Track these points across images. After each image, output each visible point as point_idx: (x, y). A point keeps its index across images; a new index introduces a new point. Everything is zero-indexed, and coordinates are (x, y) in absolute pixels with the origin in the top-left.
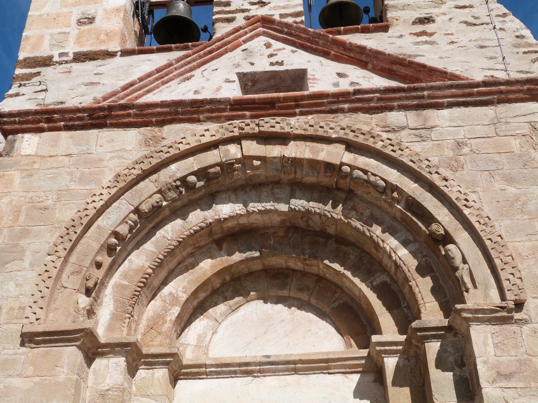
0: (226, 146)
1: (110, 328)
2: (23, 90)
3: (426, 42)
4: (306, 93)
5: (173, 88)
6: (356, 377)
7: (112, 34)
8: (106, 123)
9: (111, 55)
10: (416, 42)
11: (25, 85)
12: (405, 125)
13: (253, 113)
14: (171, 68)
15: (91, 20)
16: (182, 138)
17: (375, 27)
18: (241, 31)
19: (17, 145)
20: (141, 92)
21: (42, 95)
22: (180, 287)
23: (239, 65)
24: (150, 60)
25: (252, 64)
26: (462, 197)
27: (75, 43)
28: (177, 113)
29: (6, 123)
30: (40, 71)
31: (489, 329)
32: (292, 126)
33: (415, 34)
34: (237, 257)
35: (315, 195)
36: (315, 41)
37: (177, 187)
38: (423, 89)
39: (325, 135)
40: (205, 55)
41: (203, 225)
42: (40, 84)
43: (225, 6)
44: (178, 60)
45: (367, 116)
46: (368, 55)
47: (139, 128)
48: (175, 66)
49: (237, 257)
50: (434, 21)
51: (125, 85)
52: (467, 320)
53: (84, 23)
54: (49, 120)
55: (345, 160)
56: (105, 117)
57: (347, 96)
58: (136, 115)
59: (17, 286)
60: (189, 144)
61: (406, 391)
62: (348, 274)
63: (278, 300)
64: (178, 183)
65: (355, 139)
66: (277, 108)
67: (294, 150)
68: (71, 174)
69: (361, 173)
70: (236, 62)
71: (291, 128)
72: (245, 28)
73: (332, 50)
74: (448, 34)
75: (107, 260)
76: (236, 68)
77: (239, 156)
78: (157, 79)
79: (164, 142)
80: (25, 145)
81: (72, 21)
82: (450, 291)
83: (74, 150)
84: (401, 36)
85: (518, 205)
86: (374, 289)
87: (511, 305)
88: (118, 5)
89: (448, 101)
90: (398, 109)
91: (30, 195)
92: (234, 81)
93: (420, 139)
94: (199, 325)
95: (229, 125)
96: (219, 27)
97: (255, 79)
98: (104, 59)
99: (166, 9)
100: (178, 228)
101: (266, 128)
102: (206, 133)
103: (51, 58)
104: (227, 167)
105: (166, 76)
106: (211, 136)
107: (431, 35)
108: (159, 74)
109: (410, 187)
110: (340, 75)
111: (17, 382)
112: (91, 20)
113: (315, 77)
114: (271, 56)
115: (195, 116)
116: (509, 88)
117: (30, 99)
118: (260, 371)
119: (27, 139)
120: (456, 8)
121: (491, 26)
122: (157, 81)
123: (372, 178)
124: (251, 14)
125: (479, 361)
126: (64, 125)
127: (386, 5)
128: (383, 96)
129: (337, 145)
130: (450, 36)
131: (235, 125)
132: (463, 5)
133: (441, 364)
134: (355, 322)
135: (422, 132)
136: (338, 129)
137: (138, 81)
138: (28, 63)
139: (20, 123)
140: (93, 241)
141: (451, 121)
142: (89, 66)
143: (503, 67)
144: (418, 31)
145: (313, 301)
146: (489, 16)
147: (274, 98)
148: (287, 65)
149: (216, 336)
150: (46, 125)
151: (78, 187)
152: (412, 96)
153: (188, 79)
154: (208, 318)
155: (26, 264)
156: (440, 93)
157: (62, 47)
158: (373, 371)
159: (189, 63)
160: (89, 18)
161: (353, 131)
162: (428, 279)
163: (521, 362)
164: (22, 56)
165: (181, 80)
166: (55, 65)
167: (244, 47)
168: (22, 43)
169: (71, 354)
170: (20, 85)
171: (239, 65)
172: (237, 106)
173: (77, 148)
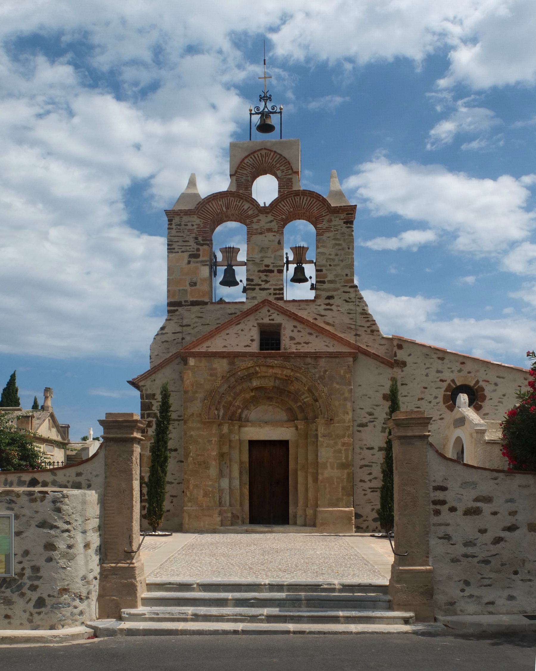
110: (295, 327)
114: (270, 316)
144: (327, 302)
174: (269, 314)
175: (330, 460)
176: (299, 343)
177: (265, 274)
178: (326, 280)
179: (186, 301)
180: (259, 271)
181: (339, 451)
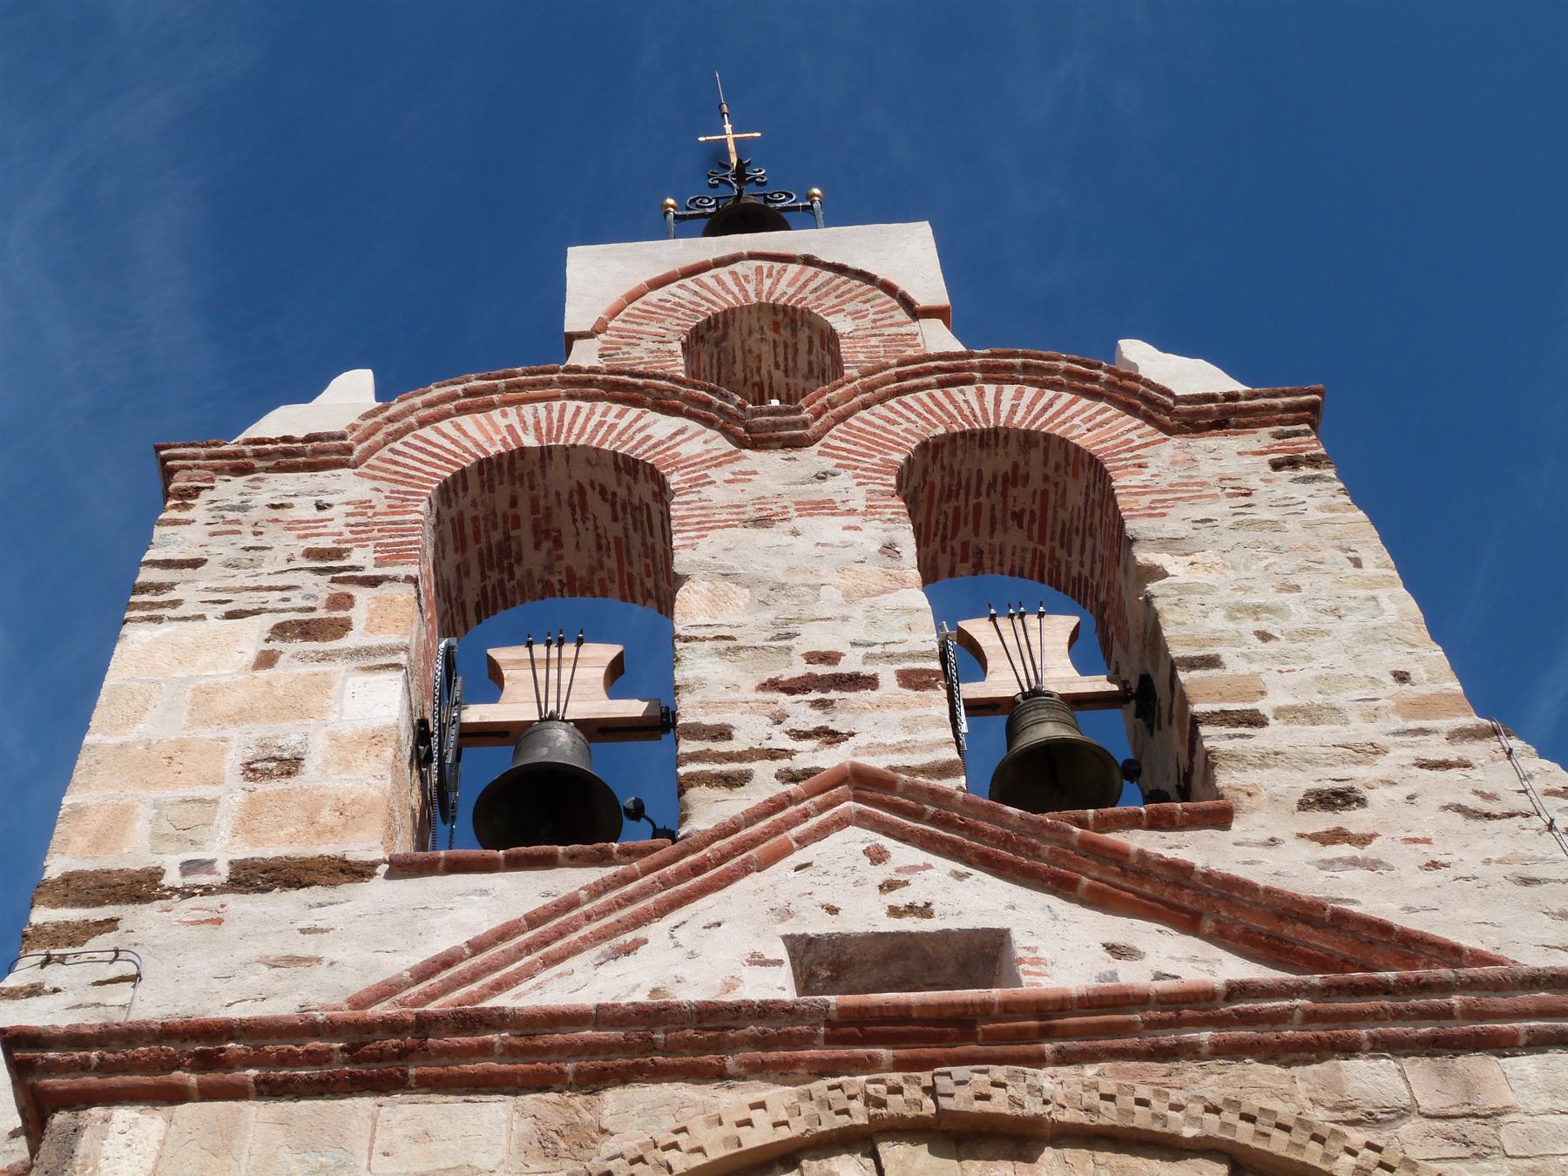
0: (824, 1161)
2: (54, 975)
3: (1354, 862)
5: (578, 976)
7: (356, 807)
8: (406, 1075)
9: (359, 872)
10: (1323, 861)
11: (62, 960)
12: (1407, 1102)
13: (902, 1053)
14: (574, 913)
15: (290, 765)
16: (677, 1132)
17: (1192, 812)
18: (792, 809)
19: (84, 1145)
21: (123, 993)
23: (789, 914)
24: (484, 892)
25: (833, 910)
27: (235, 833)
28: (649, 1047)
30: (115, 916)
32: (1047, 1096)
33: (1314, 837)
36: (1027, 845)
38: (1445, 988)
39: (1157, 1127)
40: (681, 876)
42: (115, 959)
43: (714, 739)
44: (596, 891)
45: (1277, 1070)
46: (1198, 891)
47: (516, 1094)
48: (587, 907)
50: (1362, 802)
51: (426, 964)
53: (268, 774)
54: (205, 1062)
56: (404, 1054)
57: (1204, 1004)
58: (511, 1052)
60: (700, 1150)
65: (1260, 1145)
66: (980, 1037)
70: (781, 902)
71: (1046, 1102)
72: (803, 800)
73: (1084, 874)
74: (1416, 841)
76: (783, 920)
78: (528, 948)
79: (609, 1146)
80: (113, 1144)
81: (227, 767)
84: (1273, 842)
88: (376, 724)
89: (1530, 1031)
90: (1372, 1050)
92: (779, 963)
93: (1467, 1152)
95: (831, 1088)
96: (701, 800)
97: (844, 958)
98: (333, 885)
99: (510, 750)
101: (960, 1101)
102: (756, 1115)
103: (154, 875)
105: (556, 939)
106: (776, 1125)
107: (1364, 840)
108: (536, 931)
110: (1115, 950)
112: (290, 765)
113: (1038, 954)
114: (889, 886)
115: (710, 1058)
117: (80, 1006)
119: (122, 1127)
120: (1421, 766)
121: (1538, 823)
122: (529, 953)
124: (799, 763)
126: (256, 1081)
127: (1208, 753)
128: (1320, 1006)
129: (1201, 1163)
130: (1423, 847)
131: (852, 1092)
132: (1441, 758)
135: (1468, 1126)
136: (1196, 1109)
137: (467, 951)
138: (77, 890)
139: (105, 1068)
141: (1553, 1093)
142: (284, 904)
146: (1525, 792)
147: (973, 1004)
148: (943, 915)
150: (193, 1079)
152: (1414, 1009)
153: (628, 950)
156: (1500, 1001)
157: (193, 842)
159: (630, 900)
160: (282, 760)
161: (1250, 1119)
164: (56, 867)
165: (604, 953)
166: (168, 898)
167: (799, 857)
168: (60, 827)
170: (48, 961)
171: (789, 914)
173: (303, 1161)
174: (884, 872)
177: (815, 695)
178: (1264, 706)
180: (773, 685)
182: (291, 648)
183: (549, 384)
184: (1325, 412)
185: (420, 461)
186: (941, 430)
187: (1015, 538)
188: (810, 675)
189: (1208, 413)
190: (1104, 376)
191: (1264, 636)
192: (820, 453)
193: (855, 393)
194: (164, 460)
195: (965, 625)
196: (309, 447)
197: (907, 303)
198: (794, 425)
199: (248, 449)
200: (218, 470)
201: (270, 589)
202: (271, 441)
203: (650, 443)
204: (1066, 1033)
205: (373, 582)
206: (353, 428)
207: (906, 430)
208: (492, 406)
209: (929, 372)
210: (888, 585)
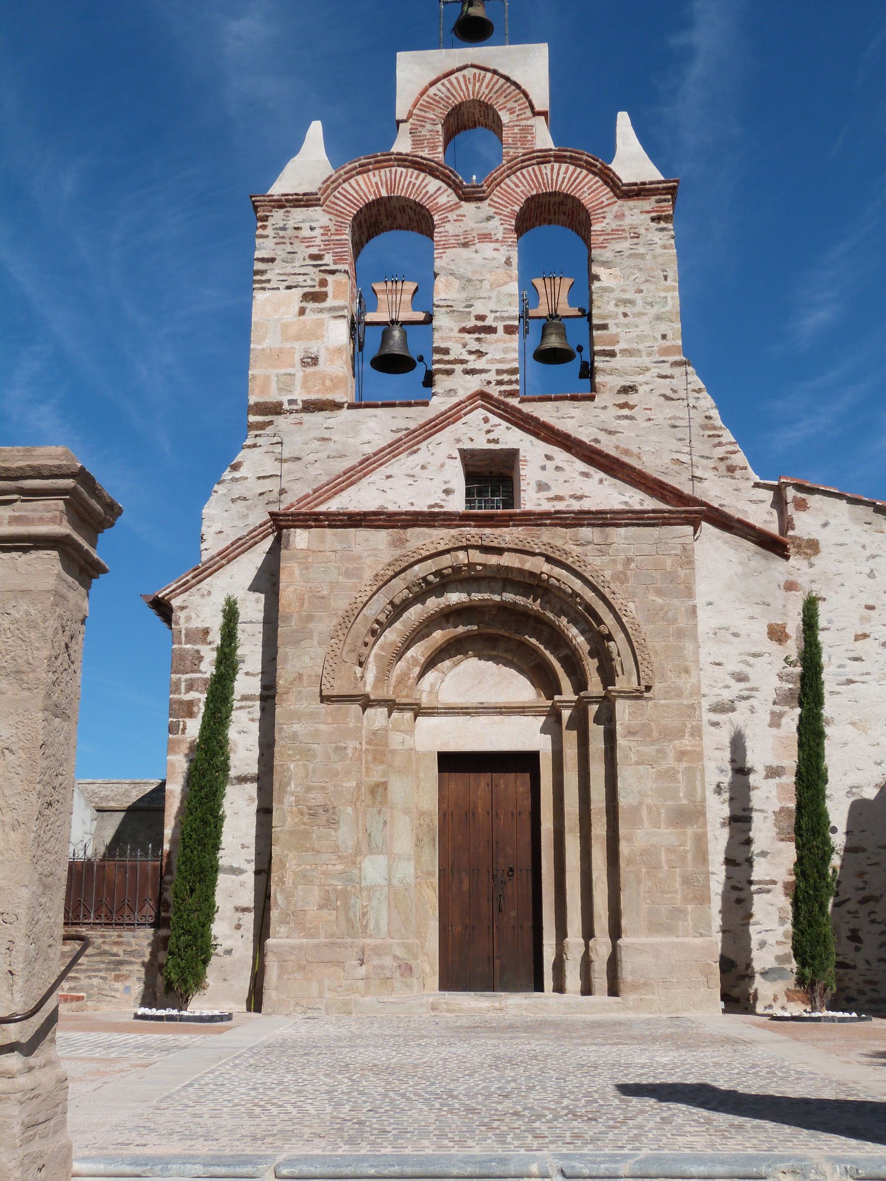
1: (375, 687)
2: (259, 441)
4: (518, 511)
6: (543, 719)
9: (338, 406)
11: (260, 435)
20: (375, 465)
22: (419, 652)
26: (623, 608)
28: (418, 520)
29: (281, 520)
31: (628, 702)
34: (461, 629)
35: (521, 591)
37: (420, 584)
40: (430, 429)
41: (437, 609)
49: (461, 629)
52: (615, 697)
54: (315, 520)
55: (544, 570)
56: (361, 520)
58: (385, 520)
59: (311, 659)
61: (575, 733)
62: (542, 647)
63: (489, 658)
64: (421, 581)
67: (507, 560)
68: (338, 568)
69: (555, 581)
70: (457, 437)
75: (370, 639)
77: (466, 562)
78: (389, 453)
82: (608, 675)
83: (338, 546)
85: (661, 614)
86: (559, 660)
87: (643, 688)
91: (309, 585)
92: (456, 458)
94: (431, 676)
100: (419, 611)
104: (456, 569)
109: (589, 595)
110: (548, 458)
111: (322, 727)
114: (488, 432)
116: (671, 515)
118: (475, 713)
123: (563, 586)
125: (618, 723)
130: (648, 412)
133: (597, 720)
134: (547, 683)
139: (292, 520)
140: (361, 627)
141: (626, 539)
143: (687, 449)
145: (515, 660)
149: (444, 684)
151: (345, 580)
153: (415, 452)
154: (437, 670)
155: (315, 643)
156: (619, 516)
158: (554, 715)
159: (416, 437)
162: (596, 660)
163: (644, 725)
167: (464, 420)
169: (356, 708)
170: (256, 436)
172: (462, 519)
174: (487, 426)
175: (649, 801)
176: (559, 498)
177: (476, 335)
178: (617, 348)
179: (291, 402)
180: (463, 330)
181: (670, 775)
182: (310, 305)
183: (390, 160)
184: (679, 189)
185: (347, 204)
186: (534, 193)
187: (562, 217)
188: (476, 326)
189: (634, 190)
190: (599, 165)
191: (625, 315)
192: (490, 205)
193: (504, 171)
194: (254, 202)
195: (534, 281)
196: (305, 198)
197: (532, 106)
198: (480, 192)
199: (283, 198)
200: (274, 207)
201: (299, 274)
202: (291, 195)
203: (428, 196)
204: (515, 520)
205: (333, 272)
206: (320, 189)
207: (522, 191)
208: (369, 170)
209: (534, 158)
210: (506, 280)
